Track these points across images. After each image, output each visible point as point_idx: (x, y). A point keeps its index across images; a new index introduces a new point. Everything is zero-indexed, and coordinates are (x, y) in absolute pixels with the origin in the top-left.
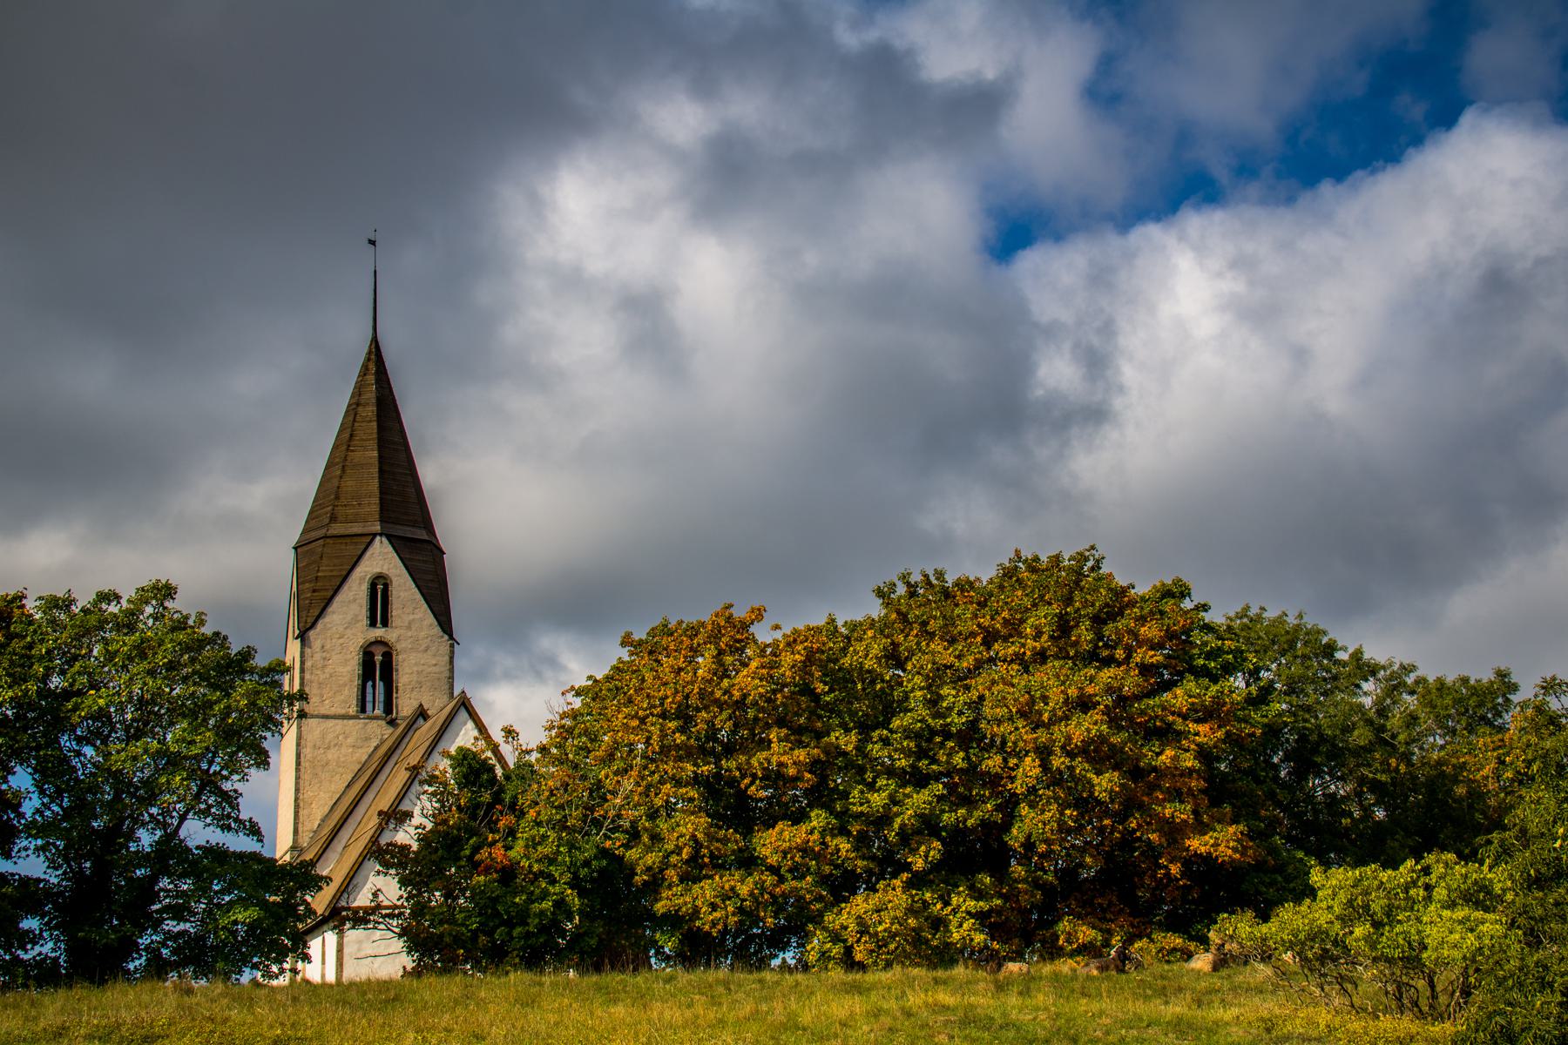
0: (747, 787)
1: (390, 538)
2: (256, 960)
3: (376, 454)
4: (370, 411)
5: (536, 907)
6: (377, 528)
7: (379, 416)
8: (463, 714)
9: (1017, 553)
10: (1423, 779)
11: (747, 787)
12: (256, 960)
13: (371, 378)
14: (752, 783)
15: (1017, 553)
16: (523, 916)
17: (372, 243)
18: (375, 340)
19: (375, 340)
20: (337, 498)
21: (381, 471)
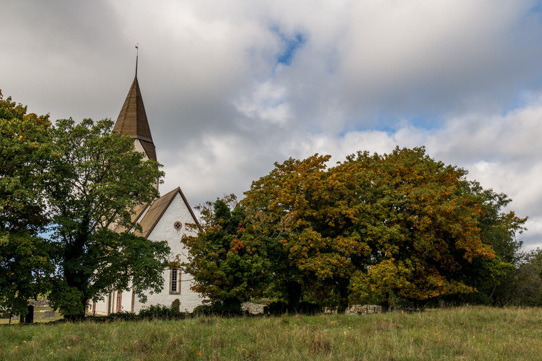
0: (328, 222)
1: (140, 140)
2: (152, 283)
3: (136, 113)
4: (134, 100)
5: (255, 265)
6: (136, 137)
7: (137, 102)
8: (179, 195)
9: (398, 147)
10: (38, 236)
11: (328, 222)
12: (152, 283)
13: (135, 90)
14: (330, 221)
15: (398, 147)
16: (249, 268)
17: (137, 47)
18: (136, 78)
19: (136, 78)
20: (123, 126)
21: (137, 119)
